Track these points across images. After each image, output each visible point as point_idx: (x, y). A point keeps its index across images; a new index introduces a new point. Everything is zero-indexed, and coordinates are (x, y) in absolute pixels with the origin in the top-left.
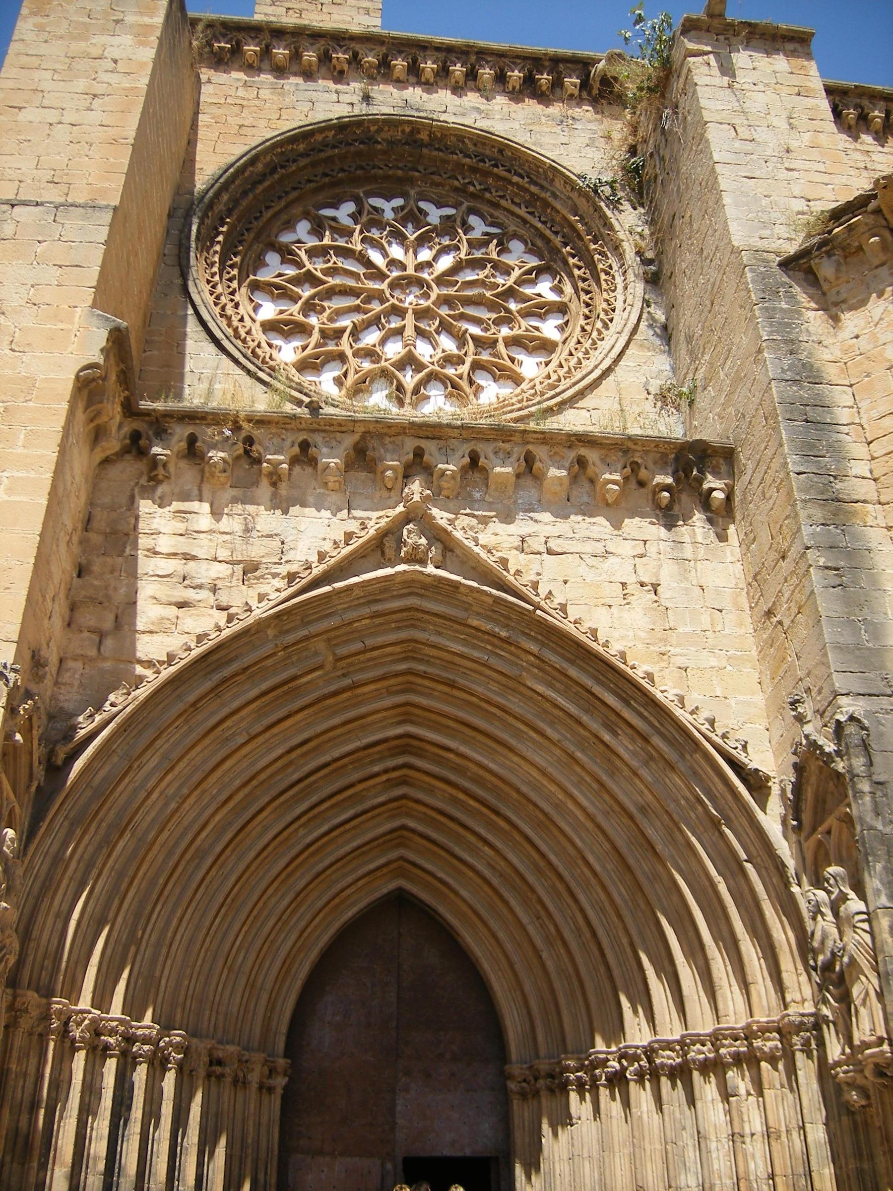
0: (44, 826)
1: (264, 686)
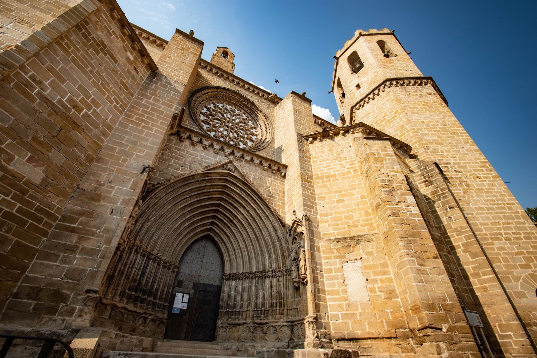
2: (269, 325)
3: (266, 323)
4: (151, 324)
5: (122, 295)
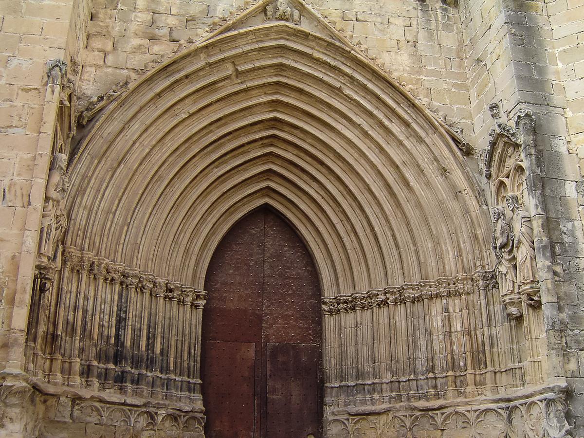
0: (77, 156)
1: (199, 86)
2: (448, 411)
3: (440, 408)
4: (167, 424)
5: (87, 372)
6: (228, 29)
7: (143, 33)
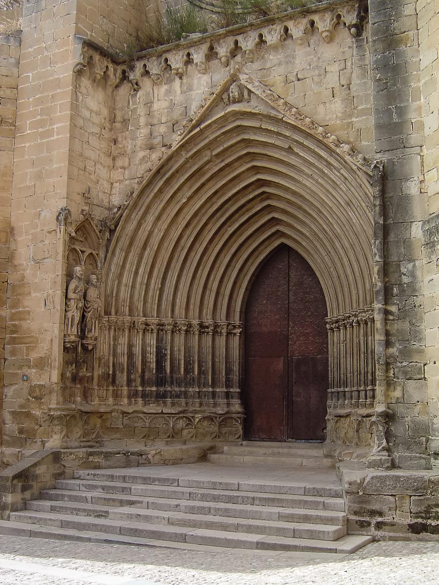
1: (186, 177)
6: (194, 127)
7: (145, 145)
